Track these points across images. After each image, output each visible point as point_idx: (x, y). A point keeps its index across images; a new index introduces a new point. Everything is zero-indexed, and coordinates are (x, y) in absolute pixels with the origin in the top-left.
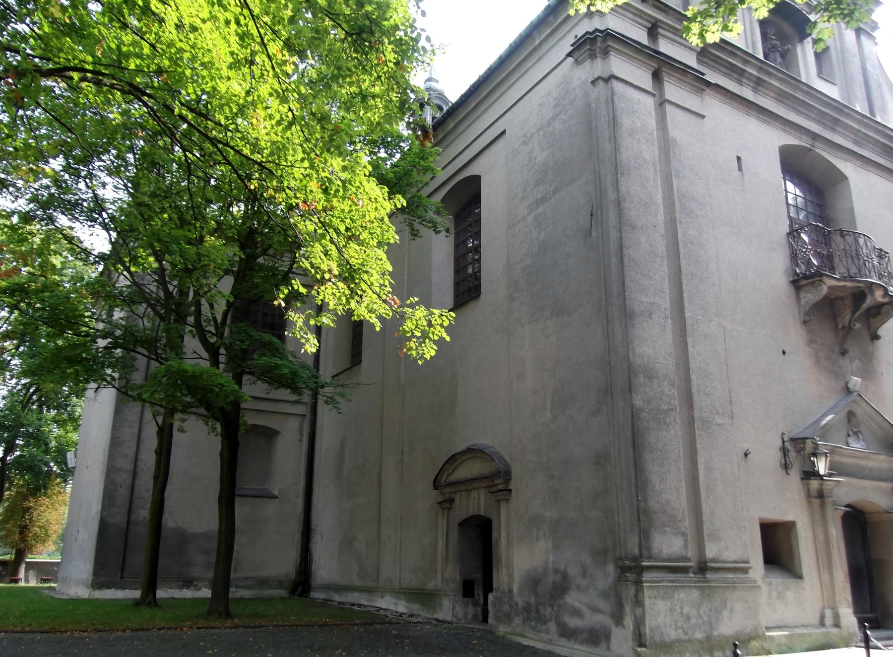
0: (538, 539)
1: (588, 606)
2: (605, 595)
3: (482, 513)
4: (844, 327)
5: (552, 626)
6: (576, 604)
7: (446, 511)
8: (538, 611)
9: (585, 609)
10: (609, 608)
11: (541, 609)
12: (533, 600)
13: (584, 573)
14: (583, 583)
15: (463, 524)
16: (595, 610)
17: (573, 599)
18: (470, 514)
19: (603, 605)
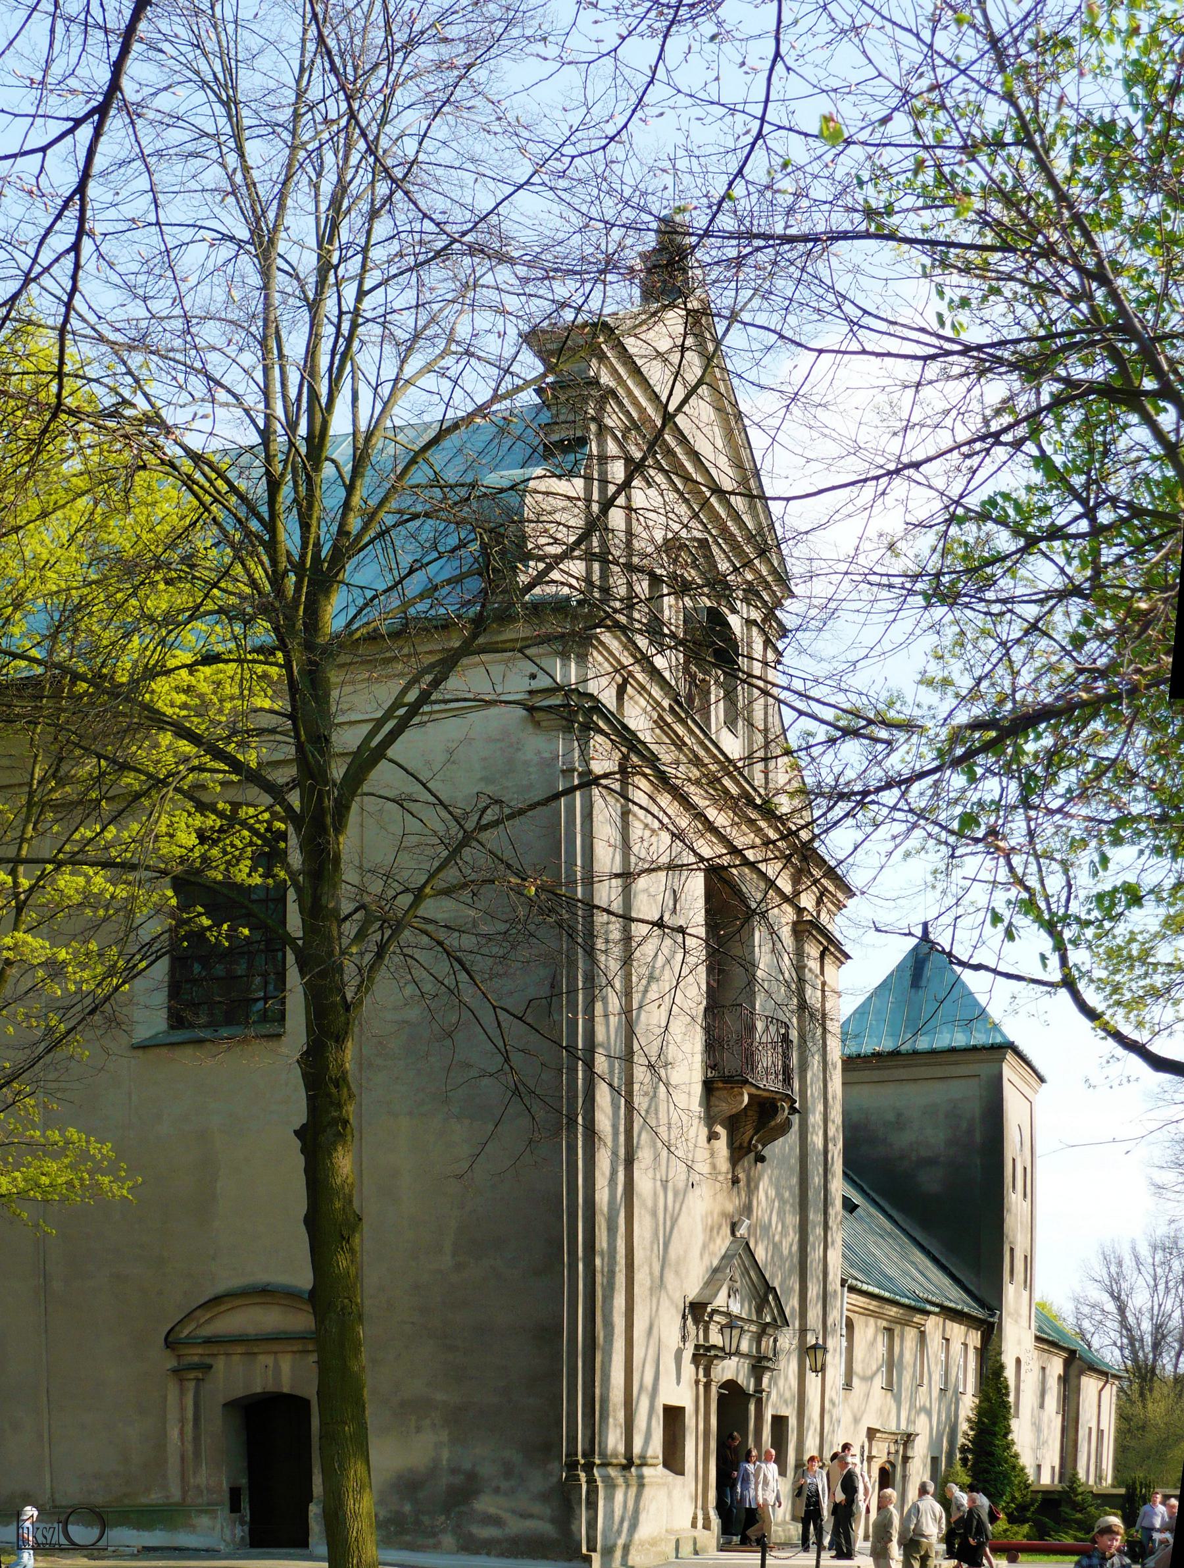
0: (419, 1429)
1: (514, 1512)
2: (544, 1497)
3: (286, 1390)
4: (741, 1147)
5: (448, 1540)
6: (492, 1510)
7: (191, 1385)
8: (418, 1522)
9: (504, 1515)
10: (548, 1511)
11: (426, 1520)
12: (407, 1508)
13: (508, 1471)
14: (504, 1485)
15: (229, 1405)
16: (525, 1516)
17: (485, 1504)
18: (259, 1390)
19: (537, 1508)
